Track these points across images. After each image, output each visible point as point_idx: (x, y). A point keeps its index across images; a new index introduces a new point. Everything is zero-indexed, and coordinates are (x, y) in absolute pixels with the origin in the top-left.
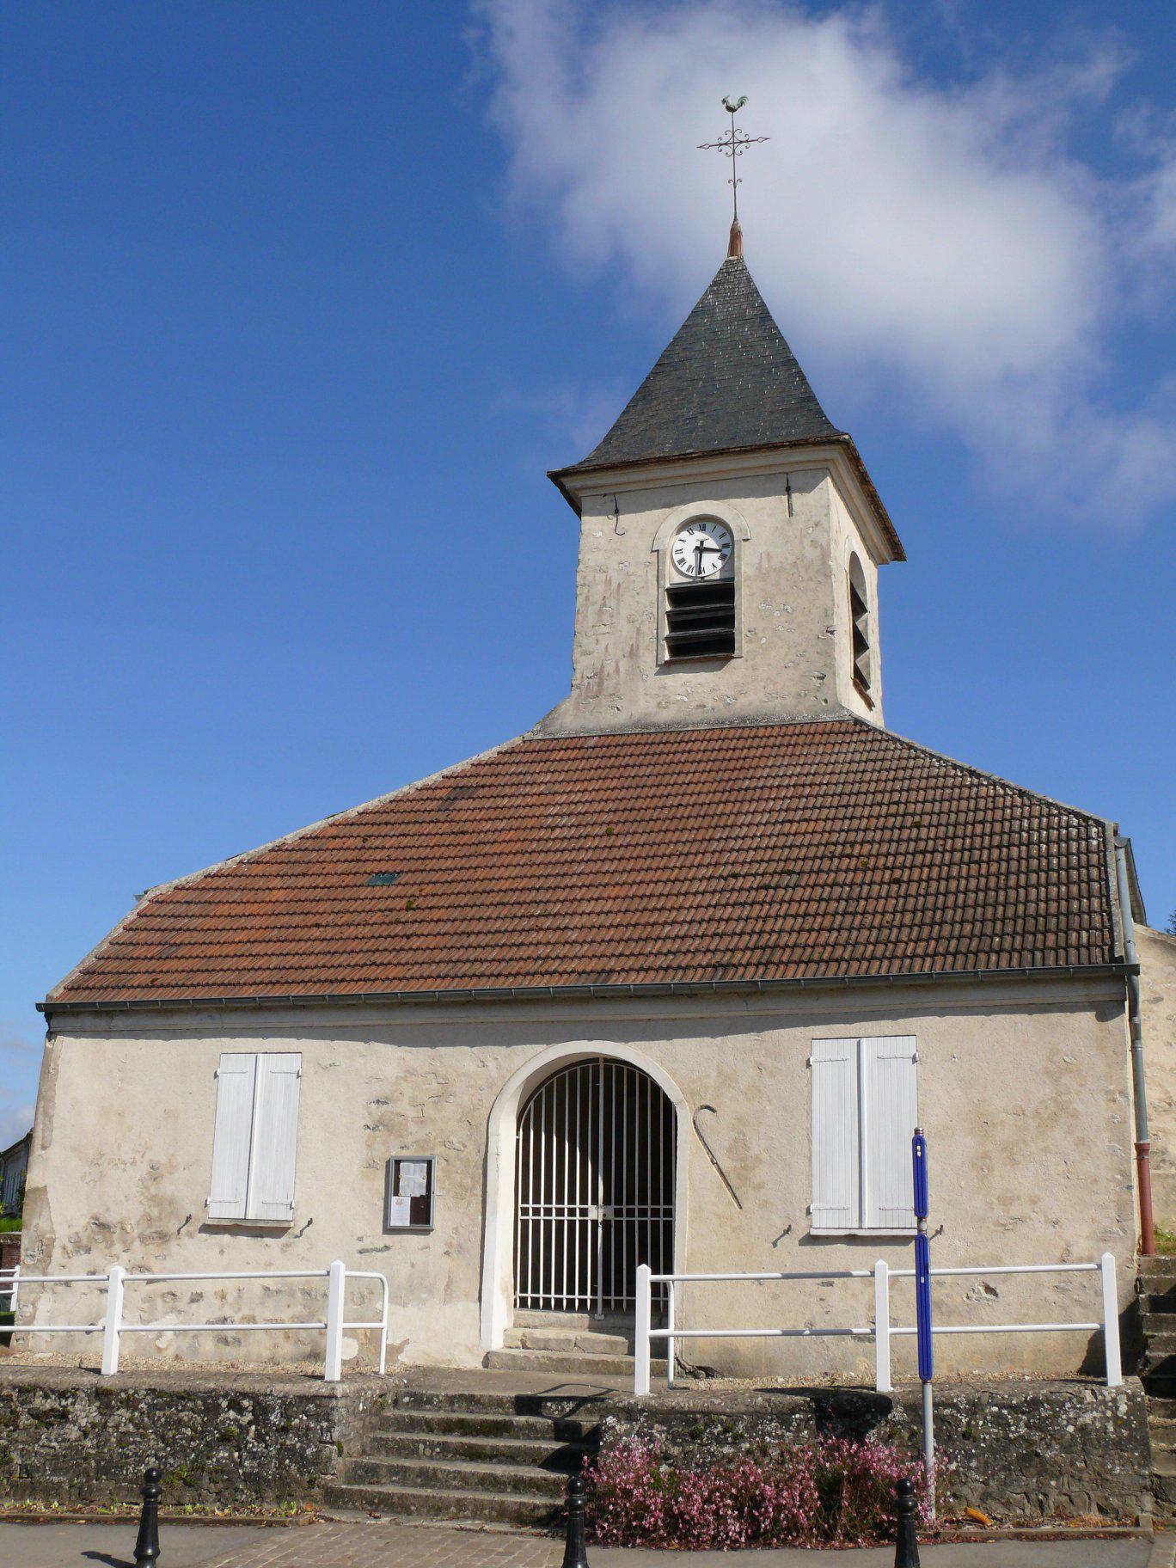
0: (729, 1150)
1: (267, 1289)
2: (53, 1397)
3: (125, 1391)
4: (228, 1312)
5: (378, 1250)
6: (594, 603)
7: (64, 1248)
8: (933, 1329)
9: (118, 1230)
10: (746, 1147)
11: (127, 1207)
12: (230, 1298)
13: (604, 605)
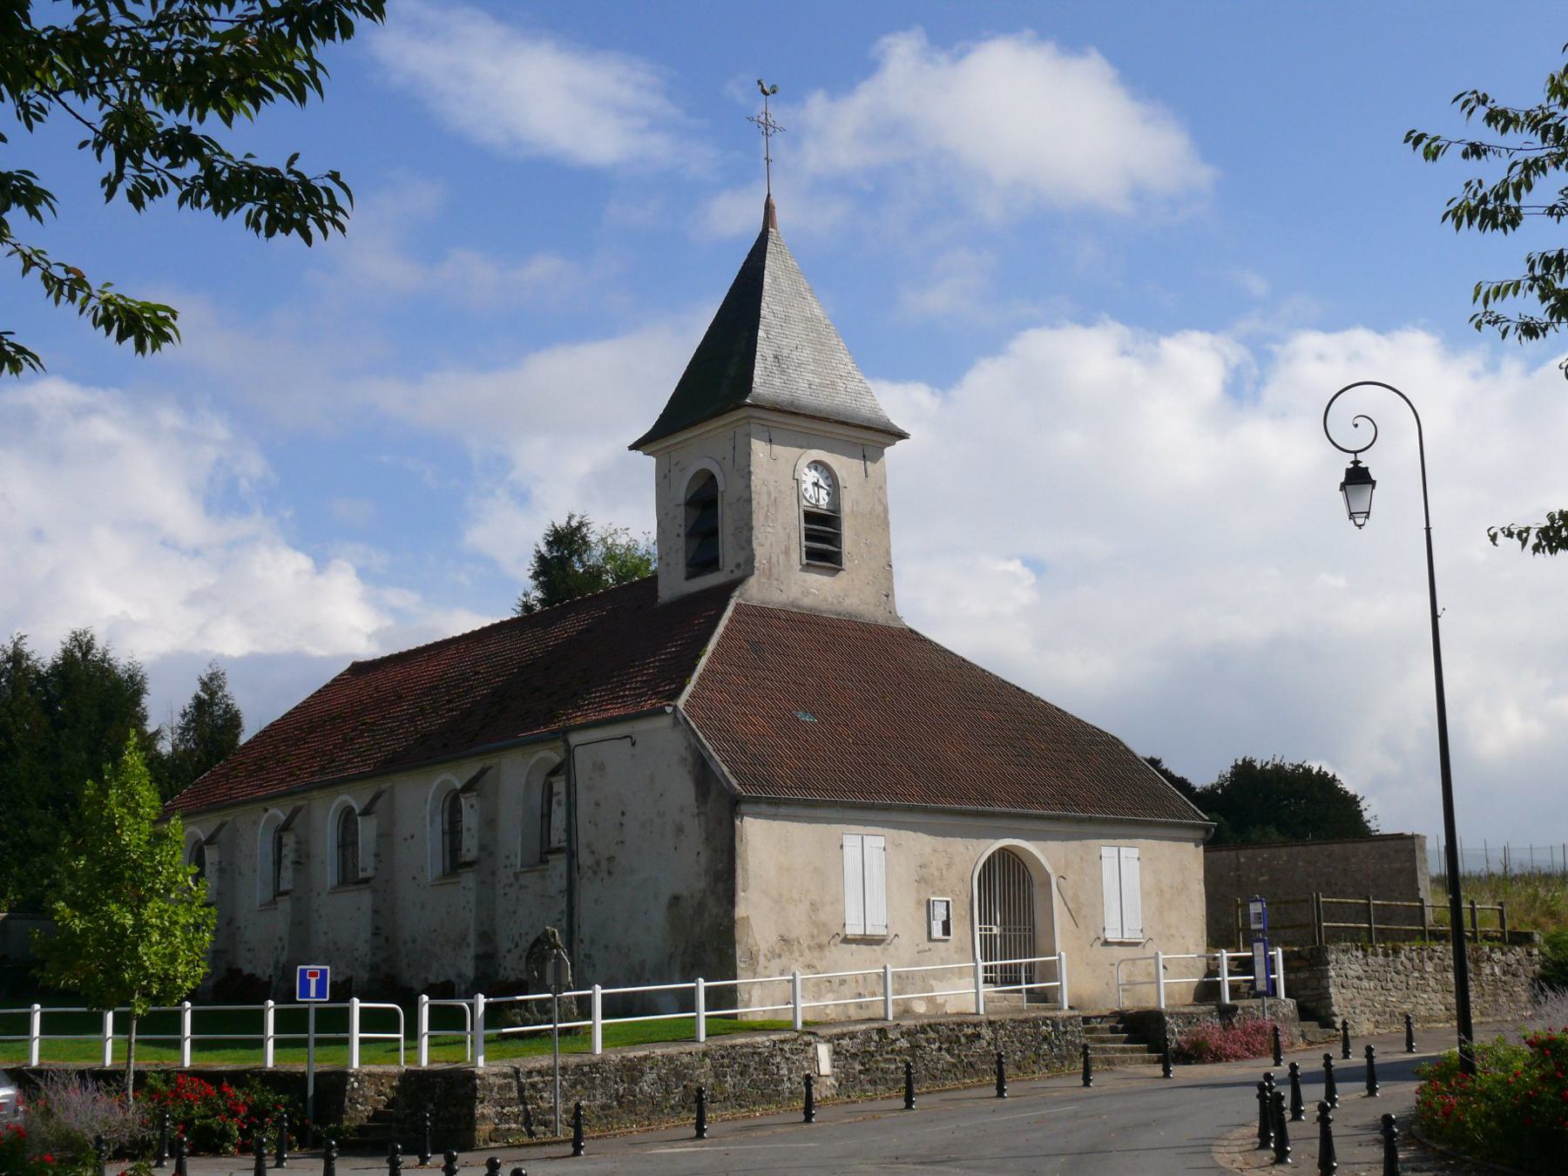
7: (765, 956)
9: (796, 943)
11: (800, 930)
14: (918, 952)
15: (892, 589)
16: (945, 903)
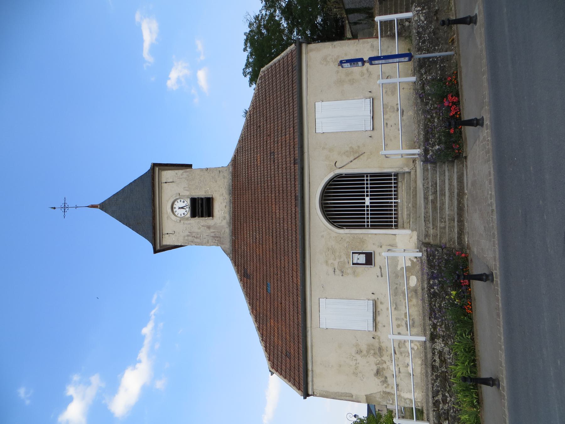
0: (348, 157)
1: (395, 308)
2: (435, 358)
3: (431, 329)
4: (404, 323)
5: (381, 270)
6: (194, 240)
7: (386, 387)
8: (397, 54)
10: (347, 151)
12: (399, 323)
13: (194, 237)
14: (382, 276)
15: (216, 168)
16: (353, 254)
